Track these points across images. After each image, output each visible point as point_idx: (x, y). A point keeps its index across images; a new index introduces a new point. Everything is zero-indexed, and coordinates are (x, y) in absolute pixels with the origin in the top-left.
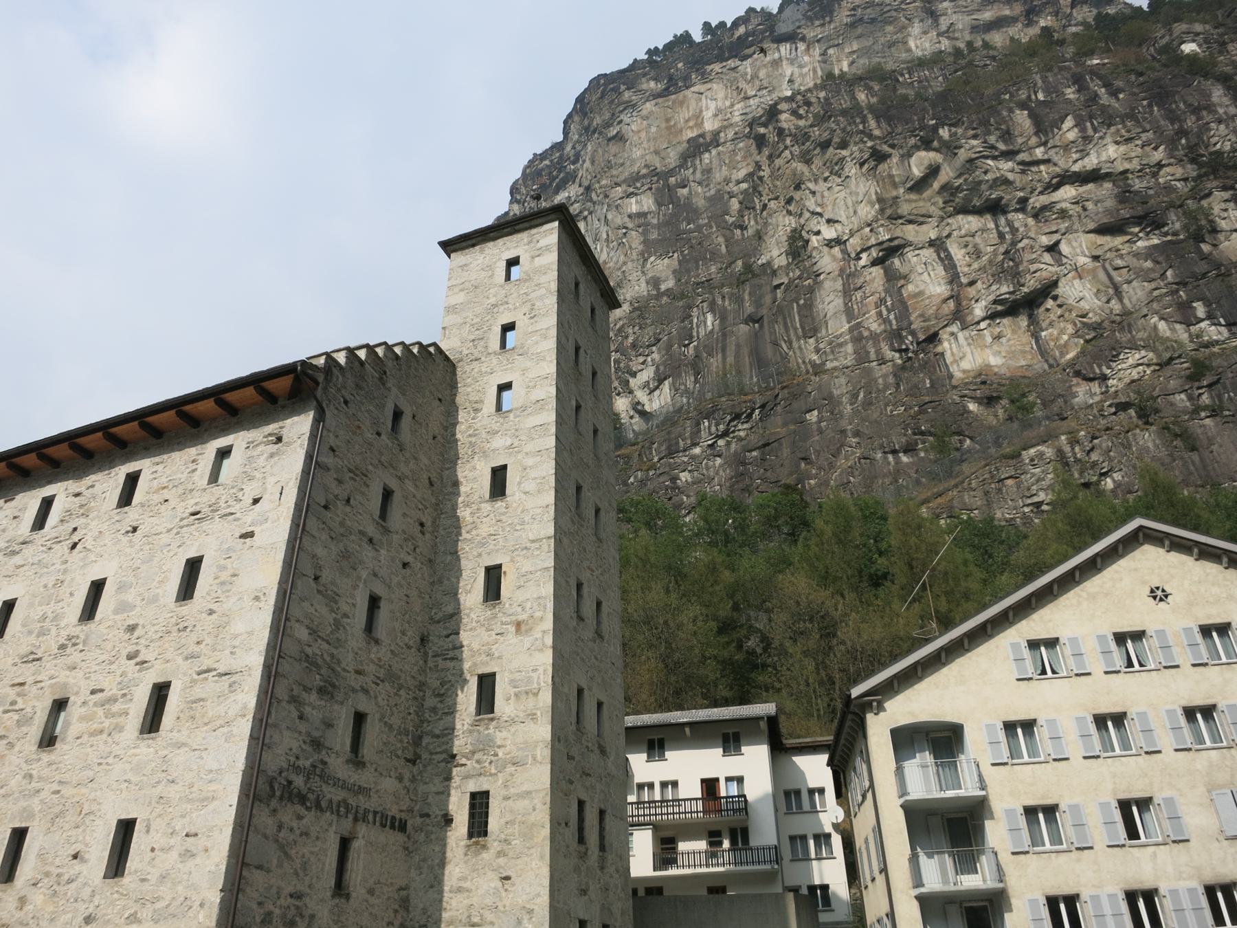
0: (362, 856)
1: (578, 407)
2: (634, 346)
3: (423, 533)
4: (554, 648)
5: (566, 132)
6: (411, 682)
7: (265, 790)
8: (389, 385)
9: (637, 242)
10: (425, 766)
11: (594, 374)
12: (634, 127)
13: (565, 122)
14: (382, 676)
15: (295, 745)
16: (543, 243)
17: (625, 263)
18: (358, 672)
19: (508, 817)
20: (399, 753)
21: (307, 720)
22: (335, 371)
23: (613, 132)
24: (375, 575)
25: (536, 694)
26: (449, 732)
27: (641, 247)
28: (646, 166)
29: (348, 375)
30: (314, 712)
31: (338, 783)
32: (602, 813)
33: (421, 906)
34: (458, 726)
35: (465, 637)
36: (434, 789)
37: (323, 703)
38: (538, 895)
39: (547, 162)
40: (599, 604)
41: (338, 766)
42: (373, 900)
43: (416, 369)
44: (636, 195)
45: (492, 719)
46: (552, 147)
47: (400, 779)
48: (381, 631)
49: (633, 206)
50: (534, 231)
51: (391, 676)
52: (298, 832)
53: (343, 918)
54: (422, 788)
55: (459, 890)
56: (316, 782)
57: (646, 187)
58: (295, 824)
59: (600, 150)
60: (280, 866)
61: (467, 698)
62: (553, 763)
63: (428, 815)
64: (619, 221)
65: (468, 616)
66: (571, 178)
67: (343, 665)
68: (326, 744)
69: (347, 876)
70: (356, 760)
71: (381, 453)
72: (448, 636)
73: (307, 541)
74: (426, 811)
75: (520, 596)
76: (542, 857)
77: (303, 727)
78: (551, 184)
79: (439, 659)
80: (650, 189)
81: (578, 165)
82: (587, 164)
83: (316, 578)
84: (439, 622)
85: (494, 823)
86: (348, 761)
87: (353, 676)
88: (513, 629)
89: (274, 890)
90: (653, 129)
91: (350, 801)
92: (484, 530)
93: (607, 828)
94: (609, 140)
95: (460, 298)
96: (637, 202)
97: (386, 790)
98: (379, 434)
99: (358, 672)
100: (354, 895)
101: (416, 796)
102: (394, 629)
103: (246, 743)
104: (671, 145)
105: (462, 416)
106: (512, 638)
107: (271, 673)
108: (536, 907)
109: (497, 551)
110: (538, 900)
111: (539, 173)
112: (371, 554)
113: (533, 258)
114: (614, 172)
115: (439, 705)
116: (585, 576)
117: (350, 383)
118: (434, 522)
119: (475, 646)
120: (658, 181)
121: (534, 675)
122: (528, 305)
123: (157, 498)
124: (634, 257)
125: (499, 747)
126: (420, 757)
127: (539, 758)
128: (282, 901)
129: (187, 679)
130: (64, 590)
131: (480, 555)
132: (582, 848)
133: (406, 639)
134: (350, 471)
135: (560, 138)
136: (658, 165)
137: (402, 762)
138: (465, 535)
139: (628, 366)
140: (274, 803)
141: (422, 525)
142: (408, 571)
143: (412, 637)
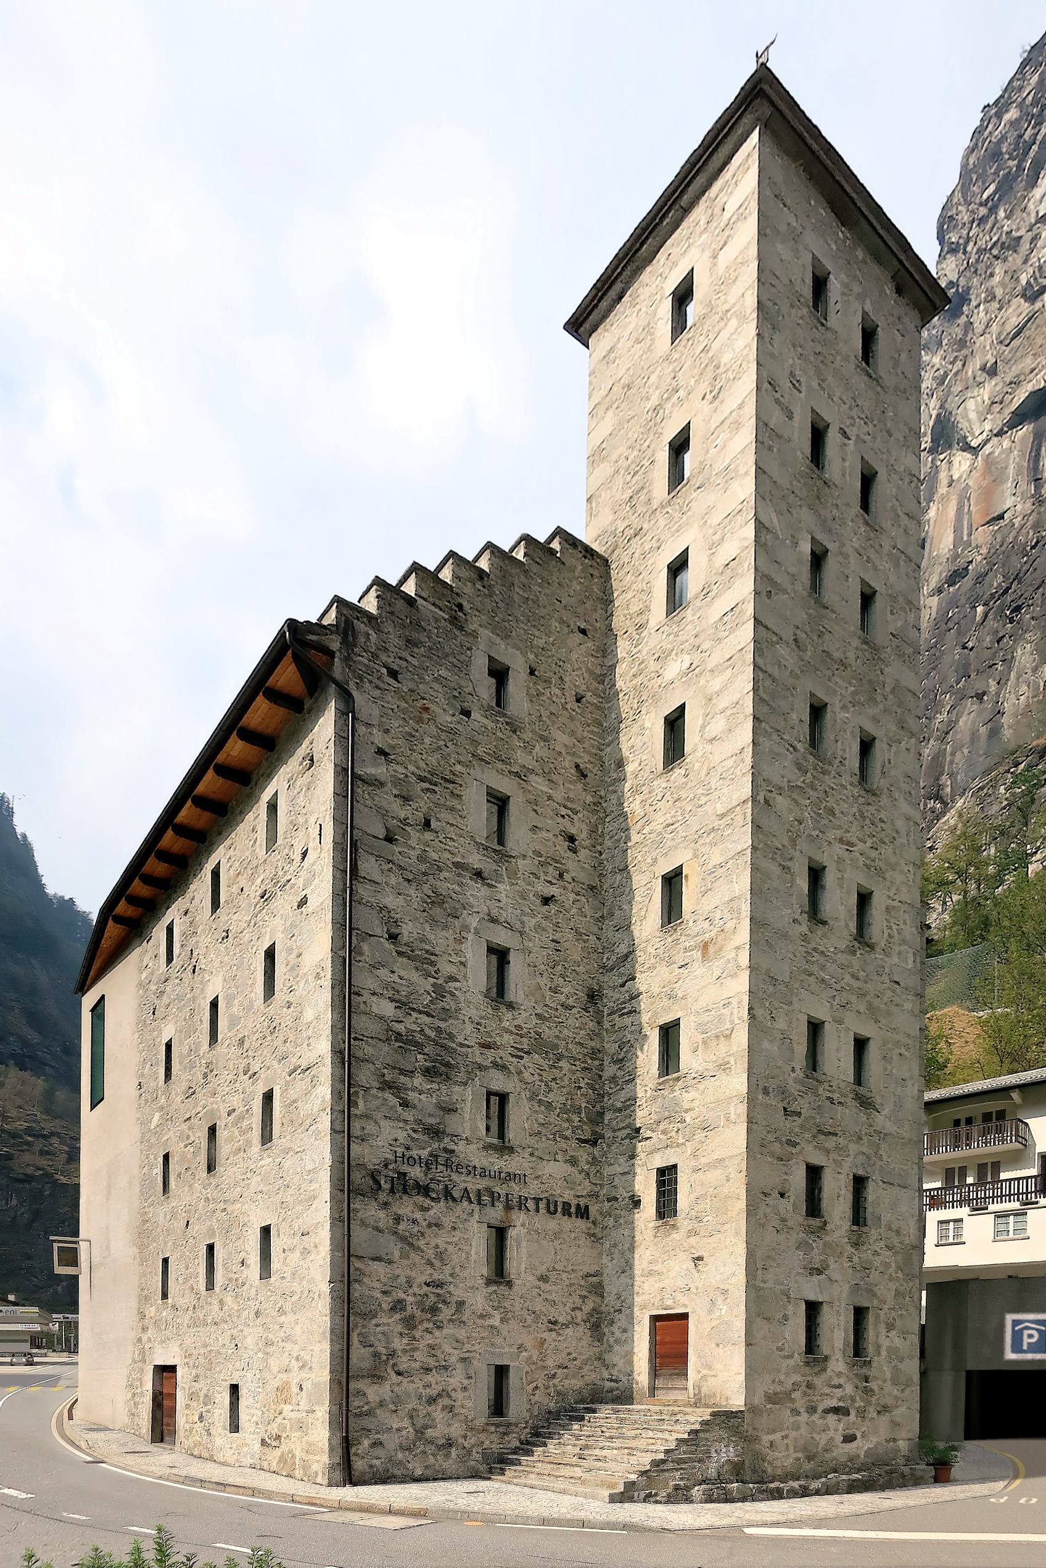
0: (524, 1244)
1: (818, 559)
4: (753, 968)
6: (575, 1050)
8: (471, 627)
10: (609, 1146)
11: (868, 481)
15: (401, 1136)
18: (487, 1046)
19: (699, 1191)
20: (568, 1133)
21: (414, 1107)
22: (360, 626)
24: (493, 920)
25: (728, 1037)
29: (389, 627)
31: (471, 1170)
34: (640, 1093)
36: (620, 1170)
37: (435, 1086)
40: (864, 899)
41: (472, 1154)
42: (546, 1287)
45: (678, 1079)
47: (573, 1162)
48: (516, 990)
51: (540, 1045)
52: (425, 1224)
54: (607, 1171)
55: (651, 1273)
58: (418, 1215)
60: (405, 1256)
69: (507, 1264)
70: (504, 1148)
71: (475, 743)
72: (623, 985)
73: (364, 891)
74: (614, 1194)
75: (707, 905)
77: (409, 1115)
79: (616, 1016)
83: (393, 937)
88: (697, 954)
92: (659, 821)
97: (555, 1175)
98: (467, 713)
99: (487, 1046)
100: (517, 1282)
105: (623, 647)
106: (698, 969)
110: (734, 1280)
112: (484, 891)
115: (620, 1073)
117: (394, 639)
118: (593, 831)
119: (655, 990)
125: (686, 1111)
127: (733, 1117)
129: (282, 1082)
130: (197, 1018)
131: (655, 860)
132: (816, 1222)
133: (562, 998)
134: (422, 779)
137: (574, 1143)
138: (635, 838)
140: (383, 1196)
141: (572, 839)
142: (553, 908)
143: (572, 991)
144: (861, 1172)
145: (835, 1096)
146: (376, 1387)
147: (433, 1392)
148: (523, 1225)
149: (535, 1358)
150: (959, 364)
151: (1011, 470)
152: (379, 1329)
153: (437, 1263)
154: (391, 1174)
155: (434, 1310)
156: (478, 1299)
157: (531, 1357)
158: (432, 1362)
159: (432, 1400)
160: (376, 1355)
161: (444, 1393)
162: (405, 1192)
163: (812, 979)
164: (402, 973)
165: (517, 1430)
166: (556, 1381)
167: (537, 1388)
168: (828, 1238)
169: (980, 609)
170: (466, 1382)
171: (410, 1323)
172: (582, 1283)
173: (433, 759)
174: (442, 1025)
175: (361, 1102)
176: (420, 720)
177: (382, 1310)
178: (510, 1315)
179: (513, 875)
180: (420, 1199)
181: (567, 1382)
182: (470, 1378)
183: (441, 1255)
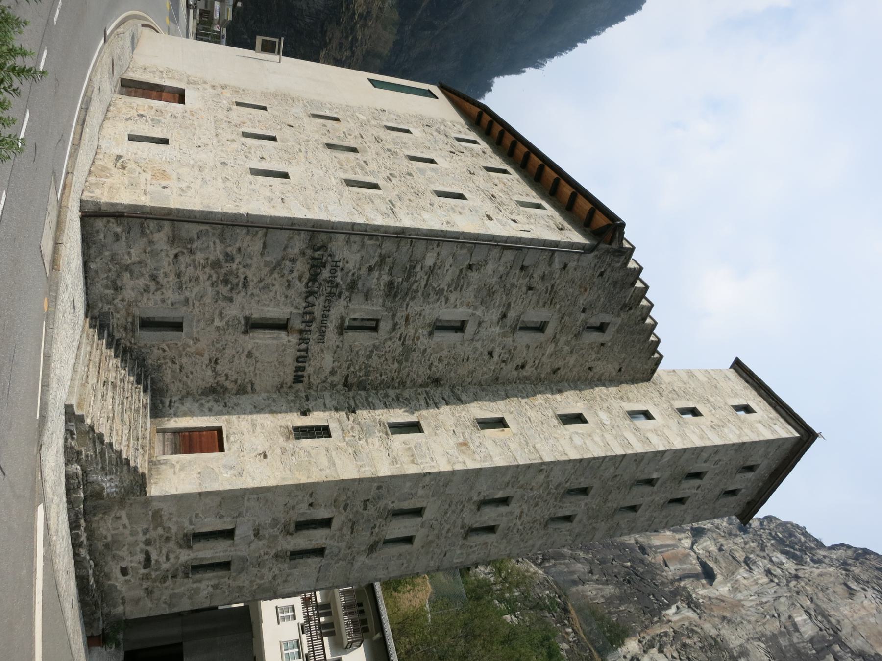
0: (275, 342)
1: (650, 482)
2: (684, 645)
3: (517, 368)
4: (453, 473)
5: (833, 548)
6: (404, 372)
7: (317, 236)
9: (772, 628)
10: (343, 394)
11: (681, 501)
12: (866, 602)
13: (842, 545)
14: (406, 343)
16: (776, 427)
17: (749, 622)
18: (407, 319)
20: (352, 369)
21: (369, 275)
22: (622, 259)
23: (854, 585)
24: (480, 324)
25: (413, 462)
26: (372, 407)
27: (768, 633)
28: (839, 622)
30: (375, 280)
31: (327, 309)
32: (320, 552)
33: (240, 402)
34: (377, 412)
35: (445, 410)
37: (382, 288)
38: (254, 479)
39: (803, 539)
40: (491, 529)
41: (338, 309)
42: (244, 356)
43: (639, 341)
44: (811, 618)
45: (387, 434)
46: (816, 540)
47: (333, 372)
48: (439, 336)
49: (800, 618)
50: (782, 420)
51: (407, 351)
52: (290, 278)
53: (230, 330)
54: (327, 394)
55: (254, 425)
56: (326, 289)
57: (821, 625)
59: (832, 579)
60: (267, 264)
61: (400, 416)
62: (360, 480)
63: (307, 400)
64: (782, 608)
65: (463, 410)
66: (800, 561)
67: (411, 304)
68: (354, 295)
71: (570, 315)
72: (443, 398)
73: (495, 252)
74: (311, 398)
75: (488, 443)
76: (284, 479)
77: (364, 271)
78: (787, 546)
80: (821, 630)
81: (812, 564)
82: (817, 572)
84: (453, 392)
85: (307, 443)
86: (343, 319)
87: (404, 314)
88: (461, 440)
89: (249, 261)
90: (872, 620)
91: (314, 325)
92: (532, 414)
93: (309, 560)
94: (845, 584)
95: (703, 378)
96: (805, 621)
97: (323, 361)
98: (584, 311)
99: (407, 319)
100: (247, 338)
101: (321, 391)
102: (442, 350)
103: (349, 221)
104: (866, 639)
105: (613, 390)
106: (452, 441)
107: (400, 235)
108: (244, 478)
109: (518, 424)
110: (249, 479)
111: (791, 535)
113: (760, 422)
114: (820, 595)
115: (390, 399)
116: (514, 506)
119: (441, 417)
120: (830, 635)
121: (428, 459)
122: (721, 423)
123: (496, 181)
124: (758, 629)
125: (366, 441)
126: (350, 390)
127: (363, 469)
128: (242, 270)
131: (511, 413)
132: (292, 528)
133: (436, 364)
134: (553, 286)
135: (827, 544)
136: (844, 632)
137: (345, 373)
138: (523, 401)
139: (666, 644)
140: (309, 252)
141: (523, 367)
142: (486, 357)
143: (440, 368)
144: (327, 552)
145: (377, 530)
146: (165, 239)
147: (161, 279)
148: (289, 341)
149: (188, 349)
150: (723, 534)
151: (685, 566)
152: (211, 244)
153: (261, 285)
154: (325, 258)
155: (226, 282)
156: (233, 311)
157: (189, 347)
158: (185, 279)
159: (154, 278)
160: (191, 241)
161: (159, 286)
162: (312, 266)
163: (447, 506)
164: (450, 272)
165: (129, 336)
166: (170, 364)
167: (164, 351)
168: (280, 537)
169: (629, 564)
170: (169, 302)
171: (216, 265)
172: (247, 380)
173: (562, 293)
174: (420, 294)
175: (372, 242)
176: (580, 287)
177: (227, 247)
178: (222, 332)
179: (504, 335)
180: (307, 276)
181: (169, 371)
182: (172, 304)
183: (267, 287)
